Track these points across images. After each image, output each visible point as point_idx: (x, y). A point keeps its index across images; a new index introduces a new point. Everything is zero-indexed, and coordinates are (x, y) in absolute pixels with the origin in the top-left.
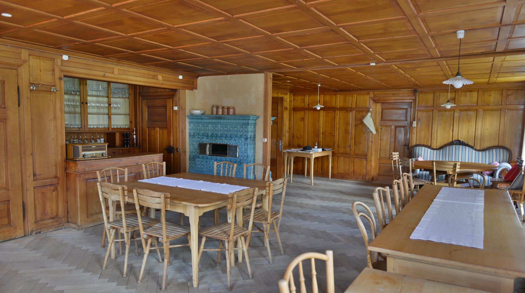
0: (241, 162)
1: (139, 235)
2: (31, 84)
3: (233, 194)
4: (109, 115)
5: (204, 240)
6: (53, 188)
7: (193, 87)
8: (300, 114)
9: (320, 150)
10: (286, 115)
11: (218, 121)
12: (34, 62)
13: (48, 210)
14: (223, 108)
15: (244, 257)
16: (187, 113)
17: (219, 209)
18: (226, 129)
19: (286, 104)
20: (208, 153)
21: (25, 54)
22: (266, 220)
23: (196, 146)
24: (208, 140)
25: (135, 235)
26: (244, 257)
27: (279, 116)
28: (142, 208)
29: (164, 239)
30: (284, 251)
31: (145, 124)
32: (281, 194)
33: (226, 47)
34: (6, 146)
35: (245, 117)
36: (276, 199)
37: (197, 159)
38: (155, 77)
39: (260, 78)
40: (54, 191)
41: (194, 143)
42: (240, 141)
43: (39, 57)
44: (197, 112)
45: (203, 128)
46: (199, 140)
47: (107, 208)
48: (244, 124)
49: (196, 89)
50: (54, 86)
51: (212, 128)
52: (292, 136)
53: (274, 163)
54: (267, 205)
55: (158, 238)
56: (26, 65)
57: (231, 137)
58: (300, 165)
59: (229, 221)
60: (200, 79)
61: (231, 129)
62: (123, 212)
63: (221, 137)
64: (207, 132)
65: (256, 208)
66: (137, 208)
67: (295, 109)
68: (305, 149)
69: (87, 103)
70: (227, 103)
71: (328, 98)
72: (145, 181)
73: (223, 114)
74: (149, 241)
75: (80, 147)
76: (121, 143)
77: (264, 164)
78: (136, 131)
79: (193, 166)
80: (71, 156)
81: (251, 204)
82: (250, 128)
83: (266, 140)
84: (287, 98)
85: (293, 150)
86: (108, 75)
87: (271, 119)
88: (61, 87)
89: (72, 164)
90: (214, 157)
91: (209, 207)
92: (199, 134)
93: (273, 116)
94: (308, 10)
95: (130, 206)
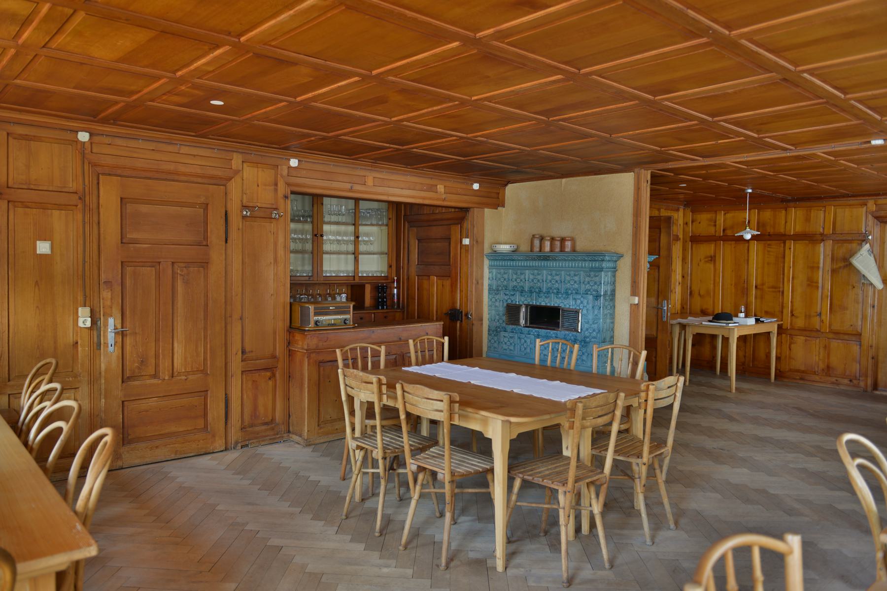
0: (585, 342)
1: (403, 465)
2: (245, 207)
3: (575, 402)
4: (356, 254)
5: (517, 483)
6: (268, 374)
7: (497, 202)
8: (707, 249)
9: (751, 321)
10: (677, 250)
11: (543, 263)
12: (249, 172)
13: (261, 409)
14: (553, 239)
15: (593, 525)
16: (487, 250)
17: (544, 428)
18: (557, 278)
19: (678, 229)
20: (522, 322)
21: (236, 160)
22: (639, 456)
23: (502, 309)
24: (523, 299)
25: (396, 461)
26: (593, 525)
27: (663, 252)
28: (408, 415)
29: (444, 475)
30: (676, 523)
31: (413, 270)
32: (671, 406)
33: (563, 128)
34: (206, 305)
35: (595, 256)
36: (661, 416)
37: (503, 334)
38: (432, 188)
39: (626, 180)
40: (270, 379)
41: (497, 304)
42: (585, 302)
43: (256, 164)
44: (505, 248)
45: (515, 277)
46: (506, 298)
47: (352, 413)
48: (592, 269)
49: (503, 206)
50: (276, 209)
51: (531, 277)
52: (690, 293)
53: (651, 343)
54: (640, 426)
55: (434, 474)
56: (238, 179)
57: (567, 293)
58: (706, 350)
59: (566, 453)
60: (510, 188)
61: (568, 278)
62: (378, 422)
63: (548, 292)
64: (522, 284)
65: (620, 432)
66: (403, 416)
67: (696, 239)
68: (718, 317)
69: (322, 236)
70: (559, 230)
71: (767, 214)
72: (414, 369)
73: (552, 250)
74: (421, 476)
75: (312, 308)
76: (376, 303)
77: (633, 343)
78: (398, 281)
79: (496, 345)
80: (297, 323)
81: (610, 424)
82: (605, 277)
83: (636, 300)
84: (680, 217)
85: (691, 320)
86: (357, 187)
87: (645, 259)
88: (285, 212)
89: (298, 336)
90: (534, 330)
91: (525, 423)
92: (506, 288)
93: (650, 253)
94: (733, 46)
95: (390, 413)
